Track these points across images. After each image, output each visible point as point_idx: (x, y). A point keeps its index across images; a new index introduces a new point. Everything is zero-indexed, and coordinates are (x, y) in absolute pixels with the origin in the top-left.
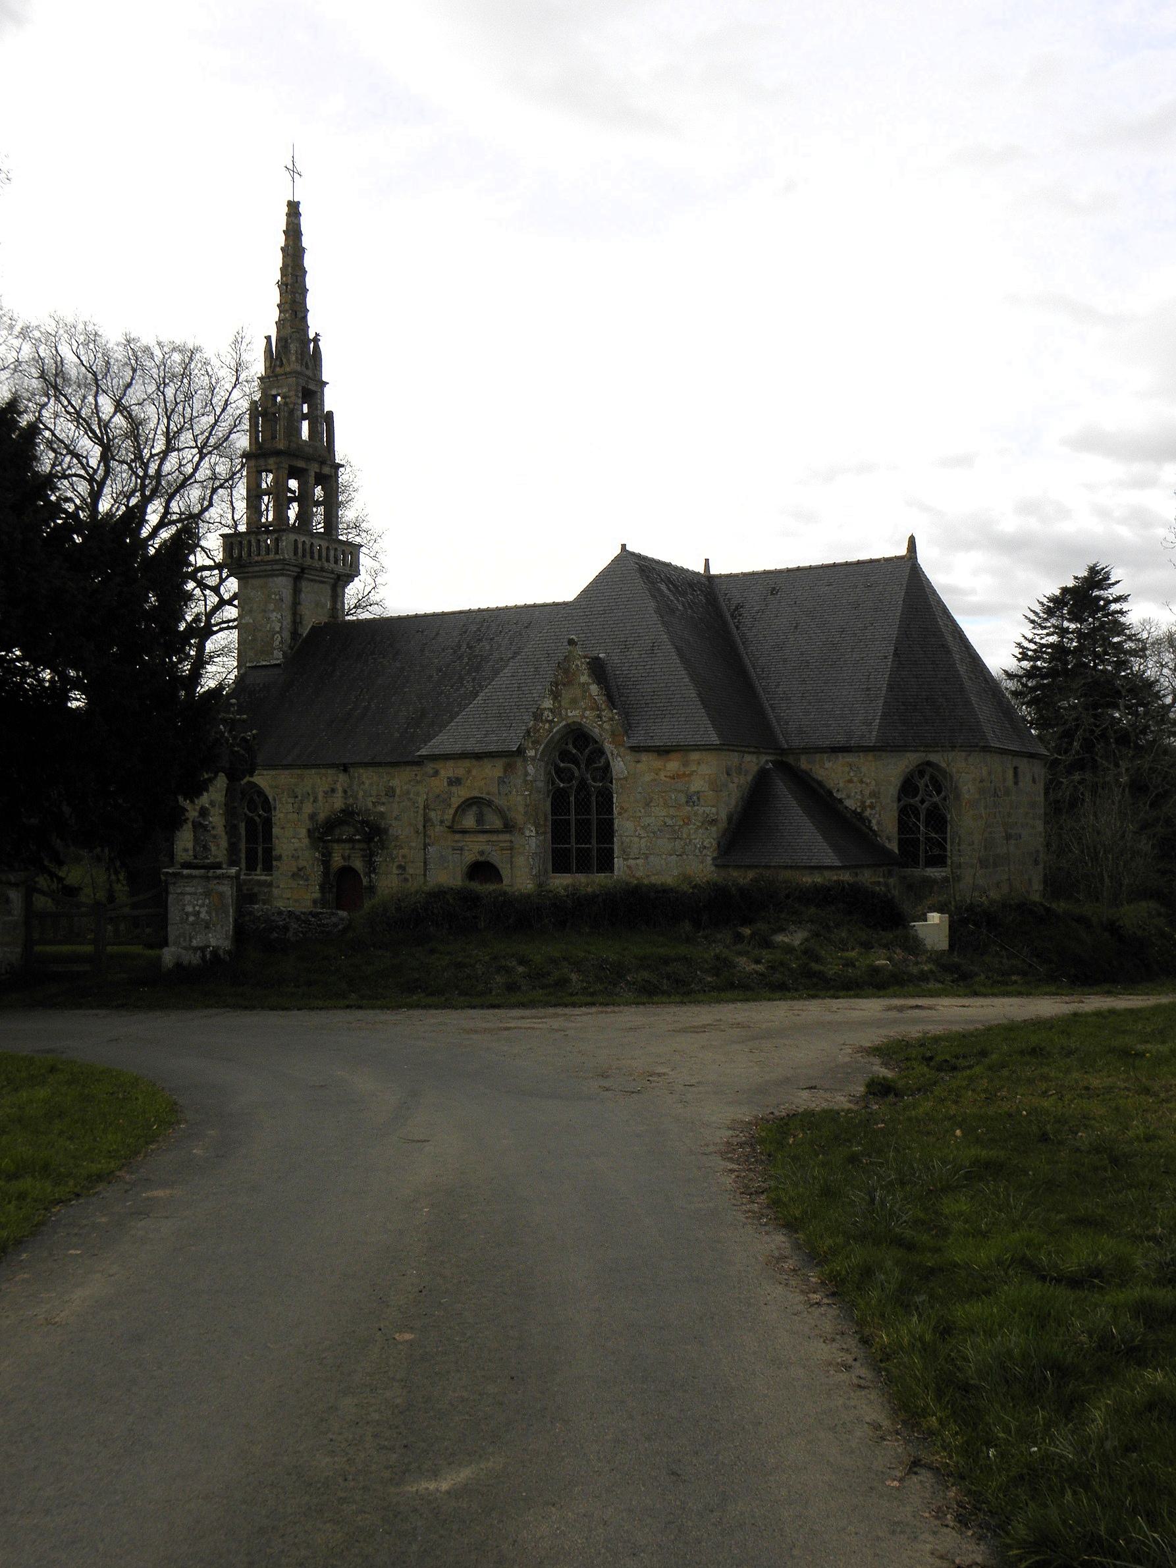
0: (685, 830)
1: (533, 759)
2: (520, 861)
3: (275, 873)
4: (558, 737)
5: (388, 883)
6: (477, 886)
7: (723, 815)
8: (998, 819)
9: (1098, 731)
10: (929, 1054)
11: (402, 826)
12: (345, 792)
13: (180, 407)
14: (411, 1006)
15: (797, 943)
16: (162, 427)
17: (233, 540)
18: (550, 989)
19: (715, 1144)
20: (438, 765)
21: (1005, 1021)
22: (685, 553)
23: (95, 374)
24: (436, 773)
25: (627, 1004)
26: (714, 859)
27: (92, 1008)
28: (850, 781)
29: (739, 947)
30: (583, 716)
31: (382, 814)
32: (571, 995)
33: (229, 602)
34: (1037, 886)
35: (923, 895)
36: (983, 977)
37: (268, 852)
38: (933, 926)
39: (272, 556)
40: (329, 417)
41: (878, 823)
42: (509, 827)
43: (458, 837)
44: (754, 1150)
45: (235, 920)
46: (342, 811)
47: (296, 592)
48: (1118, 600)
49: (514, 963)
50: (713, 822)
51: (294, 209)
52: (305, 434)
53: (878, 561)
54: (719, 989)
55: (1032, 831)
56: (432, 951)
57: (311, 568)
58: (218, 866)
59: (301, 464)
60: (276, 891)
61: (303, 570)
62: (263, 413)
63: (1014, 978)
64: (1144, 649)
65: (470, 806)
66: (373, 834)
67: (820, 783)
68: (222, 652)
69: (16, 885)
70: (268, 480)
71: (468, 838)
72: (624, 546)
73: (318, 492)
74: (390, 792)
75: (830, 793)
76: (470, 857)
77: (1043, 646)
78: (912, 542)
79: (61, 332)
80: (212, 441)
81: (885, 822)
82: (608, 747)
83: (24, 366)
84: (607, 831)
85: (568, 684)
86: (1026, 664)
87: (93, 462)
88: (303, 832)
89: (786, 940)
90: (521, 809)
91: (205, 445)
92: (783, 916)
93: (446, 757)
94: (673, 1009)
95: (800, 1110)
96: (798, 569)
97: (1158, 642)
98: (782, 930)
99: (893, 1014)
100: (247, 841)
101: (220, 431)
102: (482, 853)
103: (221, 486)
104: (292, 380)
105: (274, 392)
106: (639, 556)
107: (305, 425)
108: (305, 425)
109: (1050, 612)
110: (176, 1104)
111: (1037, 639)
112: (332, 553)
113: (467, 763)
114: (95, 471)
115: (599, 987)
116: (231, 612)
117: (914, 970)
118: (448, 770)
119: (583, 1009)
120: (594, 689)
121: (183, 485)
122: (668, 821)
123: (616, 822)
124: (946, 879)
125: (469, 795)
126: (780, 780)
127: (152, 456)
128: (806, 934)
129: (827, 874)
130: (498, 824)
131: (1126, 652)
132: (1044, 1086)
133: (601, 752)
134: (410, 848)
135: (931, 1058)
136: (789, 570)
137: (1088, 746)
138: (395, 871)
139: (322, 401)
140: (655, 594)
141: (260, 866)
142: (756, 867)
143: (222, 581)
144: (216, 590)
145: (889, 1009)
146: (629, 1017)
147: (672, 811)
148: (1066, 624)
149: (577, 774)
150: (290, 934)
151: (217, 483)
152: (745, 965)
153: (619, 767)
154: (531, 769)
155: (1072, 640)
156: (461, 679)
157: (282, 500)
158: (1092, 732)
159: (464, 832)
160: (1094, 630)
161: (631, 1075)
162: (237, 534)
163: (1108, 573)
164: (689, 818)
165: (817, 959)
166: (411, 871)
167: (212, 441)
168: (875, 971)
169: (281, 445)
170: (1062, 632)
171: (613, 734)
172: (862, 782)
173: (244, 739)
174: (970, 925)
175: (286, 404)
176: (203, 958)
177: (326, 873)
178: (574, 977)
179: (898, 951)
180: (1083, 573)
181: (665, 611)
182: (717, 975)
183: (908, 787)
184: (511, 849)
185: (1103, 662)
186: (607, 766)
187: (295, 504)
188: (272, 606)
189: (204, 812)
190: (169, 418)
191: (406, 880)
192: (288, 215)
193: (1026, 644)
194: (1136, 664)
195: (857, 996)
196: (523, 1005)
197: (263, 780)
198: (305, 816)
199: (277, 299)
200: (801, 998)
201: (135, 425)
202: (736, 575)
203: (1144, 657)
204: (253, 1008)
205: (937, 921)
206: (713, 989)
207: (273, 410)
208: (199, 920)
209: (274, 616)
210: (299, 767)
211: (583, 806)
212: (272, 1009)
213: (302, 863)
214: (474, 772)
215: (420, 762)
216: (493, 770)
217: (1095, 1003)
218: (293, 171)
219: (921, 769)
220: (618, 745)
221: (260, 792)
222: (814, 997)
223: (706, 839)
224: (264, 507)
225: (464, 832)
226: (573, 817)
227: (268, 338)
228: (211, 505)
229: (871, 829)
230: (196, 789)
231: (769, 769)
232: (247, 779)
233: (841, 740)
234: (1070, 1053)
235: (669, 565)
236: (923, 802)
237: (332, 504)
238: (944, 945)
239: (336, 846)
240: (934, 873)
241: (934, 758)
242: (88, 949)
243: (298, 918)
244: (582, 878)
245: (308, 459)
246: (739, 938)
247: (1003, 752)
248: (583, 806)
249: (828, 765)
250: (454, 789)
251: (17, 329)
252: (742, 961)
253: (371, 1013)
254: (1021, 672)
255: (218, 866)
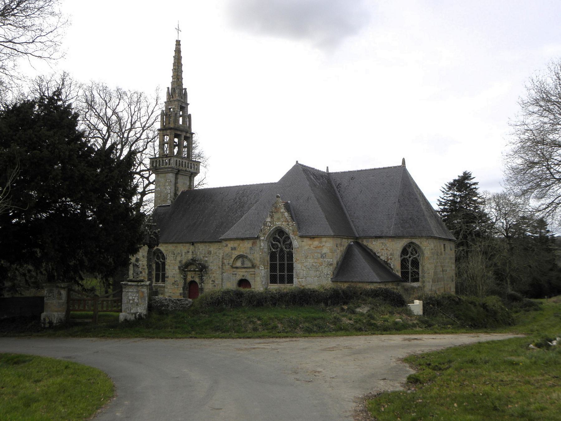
0: (320, 268)
1: (263, 240)
2: (258, 279)
3: (166, 283)
4: (272, 232)
5: (208, 287)
6: (242, 289)
7: (335, 262)
8: (438, 265)
9: (468, 232)
10: (428, 362)
11: (214, 265)
12: (193, 252)
13: (136, 113)
14: (216, 337)
15: (365, 312)
16: (129, 121)
17: (154, 160)
18: (271, 331)
19: (350, 411)
20: (228, 243)
21: (453, 346)
22: (320, 164)
23: (106, 101)
24: (227, 245)
25: (301, 337)
26: (331, 279)
27: (91, 337)
28: (383, 249)
29: (344, 313)
30: (282, 224)
31: (206, 261)
32: (278, 332)
33: (152, 183)
34: (453, 290)
35: (413, 293)
36: (437, 325)
37: (164, 275)
38: (417, 306)
39: (168, 166)
40: (190, 116)
41: (393, 265)
42: (253, 266)
43: (235, 270)
44: (367, 414)
45: (148, 302)
46: (192, 259)
47: (176, 179)
48: (475, 184)
49: (256, 320)
50: (331, 264)
51: (178, 43)
52: (181, 123)
53: (391, 167)
54: (337, 330)
55: (451, 269)
56: (224, 315)
57: (182, 170)
58: (142, 281)
59: (179, 133)
60: (166, 290)
61: (179, 171)
62: (166, 115)
63: (449, 326)
64: (484, 202)
65: (237, 260)
66: (203, 269)
67: (371, 250)
68: (149, 201)
69: (64, 288)
70: (167, 138)
71: (239, 270)
72: (297, 162)
73: (185, 143)
74: (210, 253)
75: (375, 254)
76: (239, 278)
77: (448, 200)
78: (404, 161)
79: (94, 86)
80: (147, 125)
81: (396, 265)
82: (291, 236)
83: (80, 98)
84: (291, 268)
85: (277, 212)
86: (442, 207)
87: (104, 132)
88: (177, 268)
89: (361, 311)
90: (258, 259)
91: (145, 126)
92: (360, 301)
93: (231, 240)
94: (320, 339)
95: (382, 391)
96: (361, 171)
97: (490, 199)
98: (359, 306)
99: (407, 342)
100: (156, 271)
101: (150, 122)
102: (243, 276)
103: (150, 141)
104: (176, 103)
105: (170, 107)
106: (303, 165)
107: (181, 119)
108: (181, 119)
109: (450, 188)
110: (114, 386)
111: (445, 198)
112: (190, 165)
113: (238, 242)
114: (105, 136)
115: (289, 329)
116: (152, 187)
117: (410, 323)
118: (231, 244)
119: (284, 339)
120: (286, 214)
121: (136, 141)
122: (315, 265)
123: (294, 264)
124: (419, 287)
125: (239, 254)
126: (356, 249)
127: (126, 130)
128: (368, 309)
129: (375, 285)
130: (250, 265)
131: (478, 203)
132: (483, 379)
133: (289, 238)
134: (216, 274)
135: (429, 364)
136: (358, 171)
137: (465, 237)
138: (211, 282)
139: (187, 110)
140: (309, 179)
141: (161, 280)
142: (348, 282)
143: (150, 175)
144: (147, 178)
145: (405, 340)
146: (302, 343)
147: (315, 260)
148: (455, 193)
149: (279, 246)
150: (169, 308)
151: (149, 140)
152: (346, 321)
153: (296, 243)
154: (262, 244)
155: (457, 198)
156: (236, 210)
157: (172, 145)
158: (466, 232)
159: (237, 268)
160: (466, 195)
161: (307, 372)
162: (156, 158)
163: (470, 174)
164: (322, 263)
165: (373, 318)
166: (217, 282)
167: (147, 125)
168: (396, 323)
169: (172, 126)
170: (454, 196)
171: (293, 231)
172: (387, 250)
173: (155, 232)
174: (432, 305)
175: (174, 111)
176: (135, 317)
177: (185, 283)
178: (279, 325)
179: (404, 315)
180: (461, 174)
181: (313, 185)
182: (335, 325)
183: (404, 251)
184: (254, 274)
185: (469, 206)
186: (291, 244)
187: (177, 147)
188: (167, 184)
189: (137, 260)
190: (132, 117)
191: (215, 286)
192: (176, 45)
193: (441, 200)
194: (481, 207)
195: (390, 334)
196: (260, 337)
197: (162, 248)
198: (178, 262)
199: (172, 74)
200: (368, 334)
201: (119, 119)
202: (339, 173)
203: (485, 204)
204: (153, 338)
205: (418, 303)
206: (334, 330)
207: (169, 113)
208: (134, 302)
209: (168, 187)
210: (175, 243)
211: (282, 258)
212: (161, 338)
213: (176, 279)
214: (241, 245)
215: (220, 242)
216: (248, 245)
217: (484, 337)
218: (178, 30)
219: (410, 245)
220: (295, 235)
221: (161, 253)
222: (374, 334)
223: (328, 271)
224: (165, 149)
225: (237, 268)
226: (278, 262)
227: (168, 88)
228: (146, 148)
229: (390, 267)
230: (135, 251)
231: (352, 245)
232: (156, 248)
233: (379, 234)
234: (486, 362)
235: (314, 169)
236: (410, 257)
237: (190, 148)
238: (421, 313)
239: (189, 273)
240: (415, 284)
241: (414, 241)
242: (92, 313)
243: (172, 302)
244: (282, 286)
245: (182, 131)
246: (343, 310)
247: (440, 238)
248: (282, 258)
249: (374, 243)
250: (233, 252)
251: (78, 85)
252: (344, 319)
253: (199, 340)
254: (440, 210)
255: (142, 281)
